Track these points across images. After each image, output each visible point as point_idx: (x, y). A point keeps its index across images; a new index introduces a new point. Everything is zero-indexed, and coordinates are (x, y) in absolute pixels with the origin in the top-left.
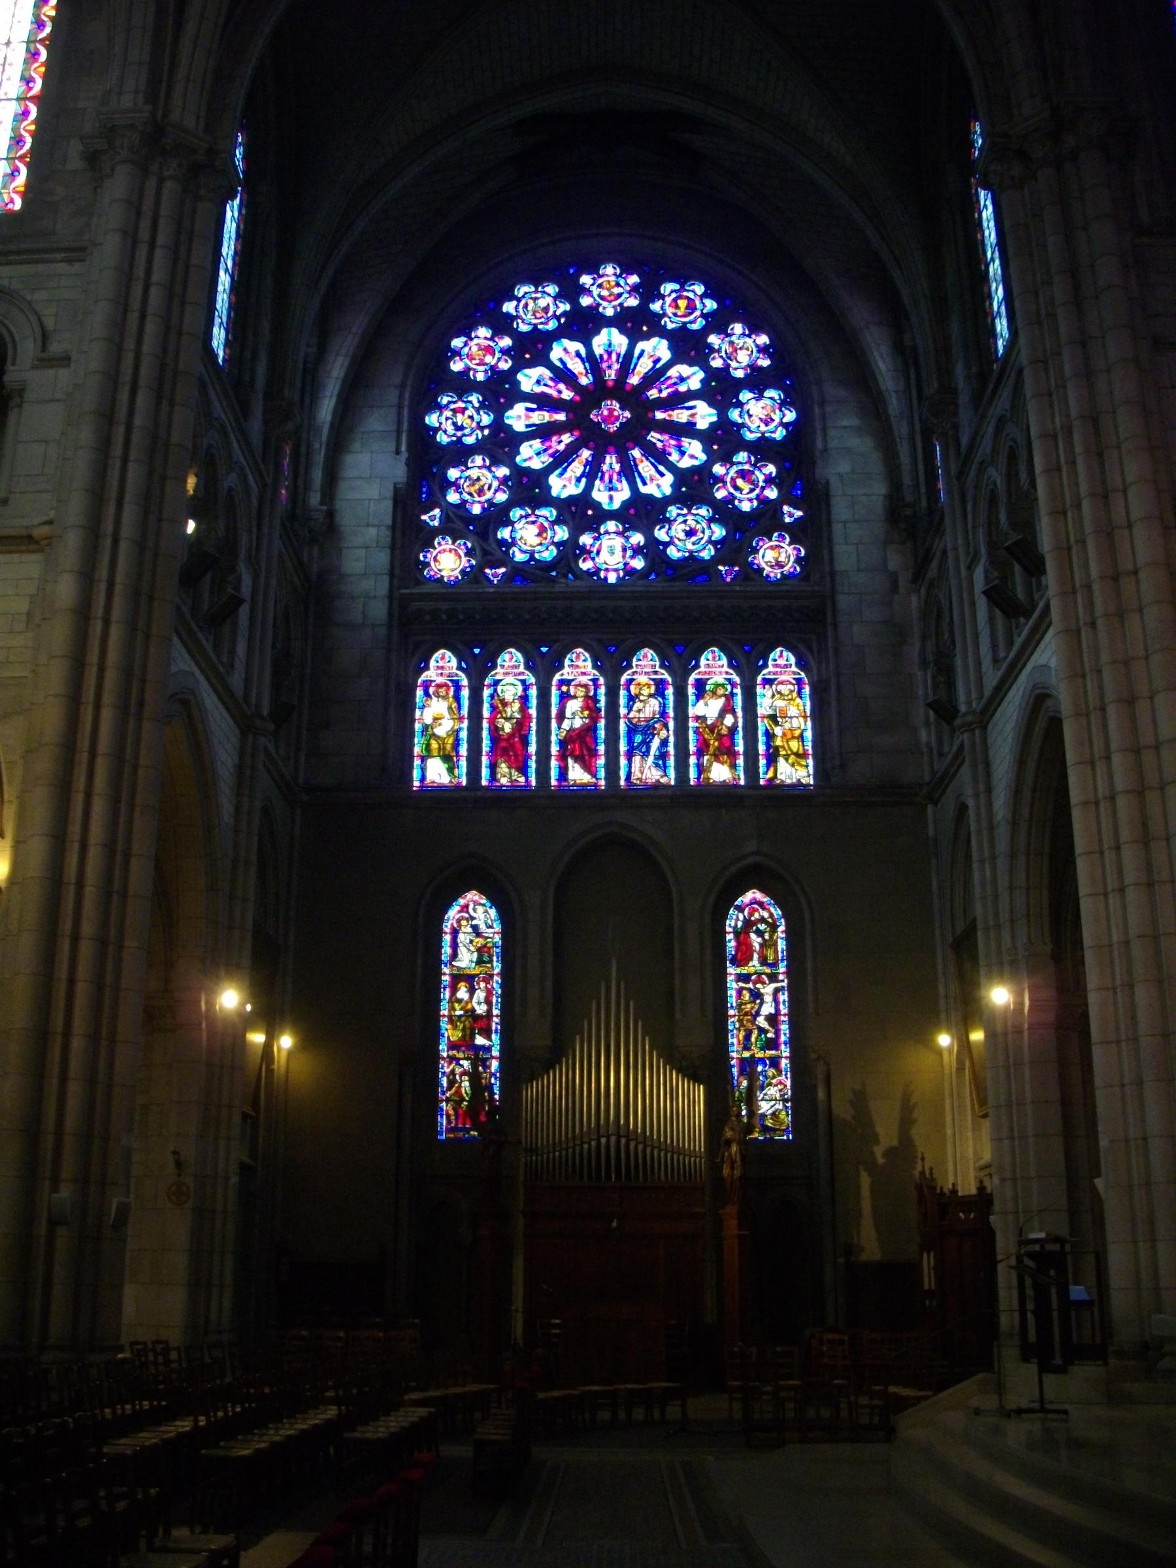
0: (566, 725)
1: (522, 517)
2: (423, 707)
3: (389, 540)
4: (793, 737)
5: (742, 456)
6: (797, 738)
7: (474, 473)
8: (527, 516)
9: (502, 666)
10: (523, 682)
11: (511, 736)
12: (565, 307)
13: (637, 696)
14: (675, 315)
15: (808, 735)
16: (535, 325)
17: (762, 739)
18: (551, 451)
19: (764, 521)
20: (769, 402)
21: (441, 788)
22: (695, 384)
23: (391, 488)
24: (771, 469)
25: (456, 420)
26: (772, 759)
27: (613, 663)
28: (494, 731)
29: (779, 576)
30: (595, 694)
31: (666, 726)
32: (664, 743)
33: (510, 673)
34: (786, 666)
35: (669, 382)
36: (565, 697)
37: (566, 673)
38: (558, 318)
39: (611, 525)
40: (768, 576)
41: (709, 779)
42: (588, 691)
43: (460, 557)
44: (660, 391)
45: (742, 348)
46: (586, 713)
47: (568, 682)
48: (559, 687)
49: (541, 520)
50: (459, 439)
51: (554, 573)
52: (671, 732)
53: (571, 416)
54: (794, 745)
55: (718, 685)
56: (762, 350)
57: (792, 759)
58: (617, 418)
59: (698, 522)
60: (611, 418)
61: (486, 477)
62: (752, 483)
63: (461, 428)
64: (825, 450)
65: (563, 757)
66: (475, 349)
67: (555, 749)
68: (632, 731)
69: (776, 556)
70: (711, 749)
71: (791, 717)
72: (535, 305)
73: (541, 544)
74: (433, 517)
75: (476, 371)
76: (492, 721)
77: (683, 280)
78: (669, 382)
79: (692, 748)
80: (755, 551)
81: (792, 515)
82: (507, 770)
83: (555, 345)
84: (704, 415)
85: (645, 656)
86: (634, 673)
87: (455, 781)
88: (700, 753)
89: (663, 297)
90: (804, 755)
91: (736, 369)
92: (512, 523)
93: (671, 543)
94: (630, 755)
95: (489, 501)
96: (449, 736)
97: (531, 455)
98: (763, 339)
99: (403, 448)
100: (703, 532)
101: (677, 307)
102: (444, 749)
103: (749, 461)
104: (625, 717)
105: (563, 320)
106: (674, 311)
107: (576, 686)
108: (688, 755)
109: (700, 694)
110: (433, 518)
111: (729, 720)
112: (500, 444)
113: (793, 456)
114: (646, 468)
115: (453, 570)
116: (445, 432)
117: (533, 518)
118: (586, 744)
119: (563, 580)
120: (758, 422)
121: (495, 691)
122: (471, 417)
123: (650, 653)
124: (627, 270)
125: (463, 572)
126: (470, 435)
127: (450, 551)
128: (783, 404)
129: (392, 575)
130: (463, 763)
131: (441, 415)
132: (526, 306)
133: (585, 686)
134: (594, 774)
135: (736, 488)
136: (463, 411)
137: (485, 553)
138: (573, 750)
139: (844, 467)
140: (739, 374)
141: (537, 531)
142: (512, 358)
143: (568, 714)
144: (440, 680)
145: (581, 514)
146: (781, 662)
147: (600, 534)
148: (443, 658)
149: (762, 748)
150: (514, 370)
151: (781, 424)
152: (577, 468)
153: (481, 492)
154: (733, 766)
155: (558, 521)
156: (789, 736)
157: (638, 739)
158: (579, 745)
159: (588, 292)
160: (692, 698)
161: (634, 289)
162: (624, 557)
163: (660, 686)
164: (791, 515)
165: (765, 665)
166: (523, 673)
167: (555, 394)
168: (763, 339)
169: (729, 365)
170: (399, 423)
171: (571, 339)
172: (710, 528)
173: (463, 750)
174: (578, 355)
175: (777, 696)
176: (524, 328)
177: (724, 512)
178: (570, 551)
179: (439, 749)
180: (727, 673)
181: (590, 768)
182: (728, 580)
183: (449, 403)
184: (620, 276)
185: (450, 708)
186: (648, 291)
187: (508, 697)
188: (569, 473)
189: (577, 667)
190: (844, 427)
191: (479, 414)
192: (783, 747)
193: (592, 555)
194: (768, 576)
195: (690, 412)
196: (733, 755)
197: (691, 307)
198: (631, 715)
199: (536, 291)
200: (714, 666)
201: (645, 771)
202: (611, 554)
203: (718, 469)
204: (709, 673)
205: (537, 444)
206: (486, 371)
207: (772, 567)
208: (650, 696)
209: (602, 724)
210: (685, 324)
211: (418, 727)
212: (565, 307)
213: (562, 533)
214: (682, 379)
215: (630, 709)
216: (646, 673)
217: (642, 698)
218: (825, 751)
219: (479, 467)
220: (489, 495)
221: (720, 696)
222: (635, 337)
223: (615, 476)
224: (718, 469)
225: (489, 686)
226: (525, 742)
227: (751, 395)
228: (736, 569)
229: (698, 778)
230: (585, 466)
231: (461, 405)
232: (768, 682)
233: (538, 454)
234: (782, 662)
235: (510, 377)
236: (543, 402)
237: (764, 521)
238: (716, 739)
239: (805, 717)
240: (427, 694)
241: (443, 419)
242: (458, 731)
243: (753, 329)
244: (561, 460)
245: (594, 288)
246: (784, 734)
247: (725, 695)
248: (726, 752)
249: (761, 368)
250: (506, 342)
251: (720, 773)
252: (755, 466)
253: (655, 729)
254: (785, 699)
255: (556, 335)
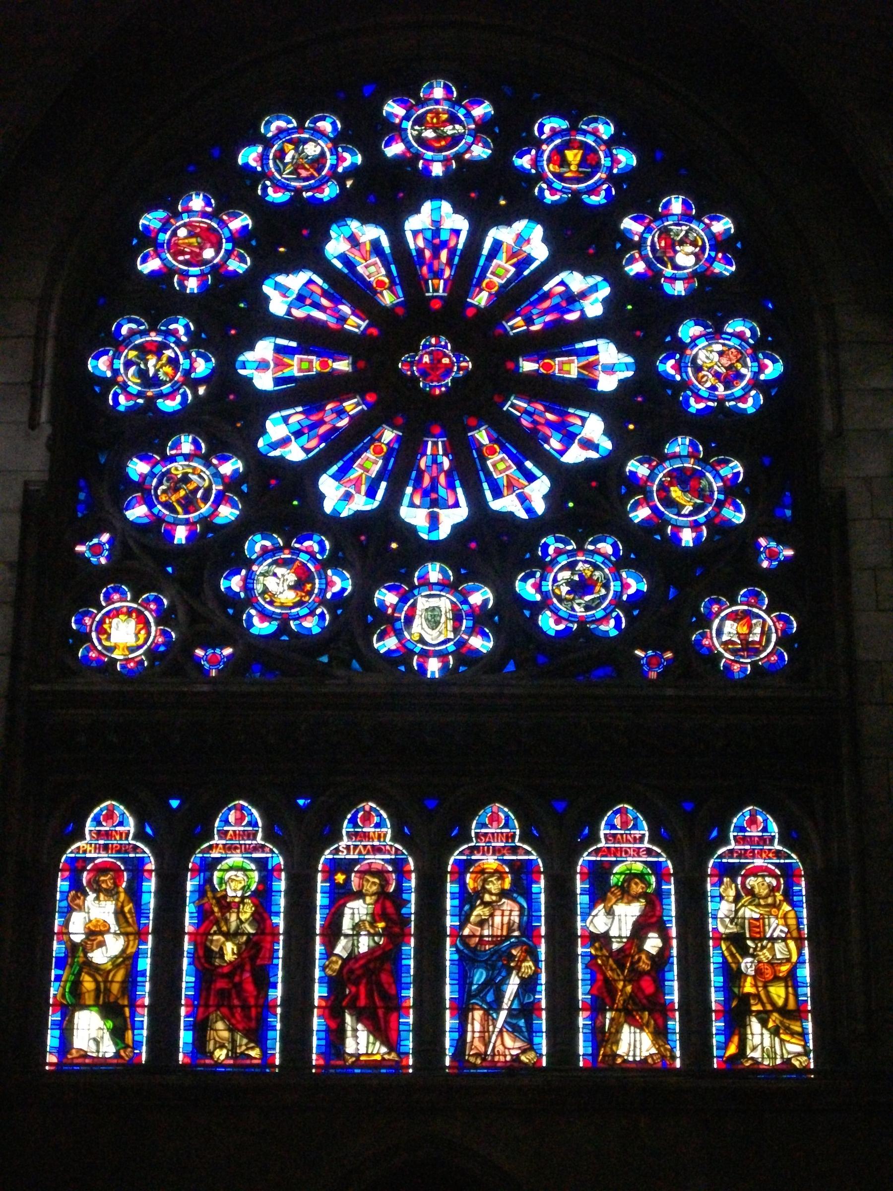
0: (341, 948)
1: (265, 552)
2: (70, 910)
3: (12, 589)
4: (776, 979)
5: (680, 445)
6: (784, 979)
7: (178, 468)
8: (277, 550)
9: (223, 834)
10: (262, 864)
11: (237, 966)
12: (352, 159)
13: (479, 894)
14: (560, 177)
15: (805, 973)
16: (298, 191)
17: (716, 980)
18: (322, 430)
19: (723, 565)
20: (734, 342)
21: (95, 1068)
22: (593, 308)
23: (18, 490)
24: (736, 467)
25: (144, 367)
26: (736, 1023)
27: (433, 833)
28: (205, 957)
29: (404, 962)
30: (399, 889)
31: (532, 954)
32: (528, 985)
33: (238, 859)
34: (762, 840)
35: (546, 304)
36: (341, 895)
37: (344, 846)
38: (341, 179)
39: (434, 572)
40: (727, 668)
41: (615, 1056)
42: (385, 883)
43: (147, 624)
44: (529, 321)
45: (687, 244)
46: (381, 925)
47: (347, 866)
48: (329, 877)
49: (304, 558)
50: (151, 402)
51: (325, 659)
52: (543, 965)
53: (362, 364)
54: (778, 992)
55: (631, 876)
56: (719, 243)
57: (775, 1019)
58: (448, 370)
59: (596, 567)
60: (435, 370)
61: (201, 476)
62: (699, 493)
63: (155, 382)
64: (839, 432)
65: (334, 1010)
66: (182, 233)
67: (319, 991)
68: (469, 958)
69: (740, 631)
70: (620, 1000)
71: (772, 940)
72: (294, 153)
73: (300, 604)
74: (96, 549)
75: (185, 275)
76: (201, 938)
77: (575, 115)
78: (546, 304)
79: (582, 993)
80: (705, 621)
81: (771, 552)
82: (226, 1034)
83: (334, 231)
84: (612, 365)
85: (494, 818)
86: (473, 850)
87: (126, 1054)
88: (596, 1008)
89: (538, 144)
90: (798, 1014)
91: (673, 279)
92: (248, 563)
93: (545, 603)
94: (462, 1010)
95: (203, 520)
96: (116, 966)
97: (283, 436)
98: (723, 225)
99: (44, 415)
100: (606, 586)
101: (564, 163)
102: (108, 991)
103: (694, 455)
104: (457, 932)
105: (349, 184)
106: (557, 169)
107: (362, 873)
108: (573, 1011)
109: (600, 891)
110: (97, 550)
111: (653, 944)
112: (228, 414)
113: (778, 447)
114: (500, 465)
115: (132, 650)
116: (124, 387)
117: (286, 555)
118: (379, 984)
119: (341, 672)
120: (711, 381)
121: (209, 881)
122: (173, 362)
123: (504, 811)
124: (471, 93)
125: (152, 653)
126: (170, 396)
127: (129, 612)
128: (759, 347)
129: (15, 657)
130: (143, 1018)
131: (117, 356)
132: (281, 154)
133: (380, 874)
134: (393, 1045)
135: (670, 503)
136: (159, 349)
137: (194, 617)
138: (355, 997)
139: (874, 464)
140: (679, 289)
141: (292, 578)
142: (251, 251)
143: (347, 925)
144: (103, 857)
145: (379, 549)
146: (754, 833)
147: (413, 587)
148: (110, 816)
149: (715, 997)
150: (257, 276)
151: (755, 383)
152: (371, 463)
153: (189, 504)
154: (660, 1034)
155: (335, 561)
156: (769, 975)
157: (479, 976)
158: (366, 988)
159: (397, 132)
160: (582, 900)
161: (483, 128)
162: (456, 630)
163: (522, 875)
164: (772, 556)
165: (723, 840)
166: (262, 848)
167: (331, 321)
168: (723, 225)
169: (660, 274)
170: (38, 367)
171: (364, 221)
172: (618, 578)
173: (145, 990)
174: (376, 245)
175: (746, 899)
176: (276, 197)
177: (647, 548)
178: (355, 619)
179: (97, 990)
180: (649, 852)
181: (382, 1031)
182: (653, 675)
183: (132, 333)
184: (457, 103)
185: (119, 913)
186: (509, 132)
187: (233, 892)
188: (356, 472)
189: (366, 836)
190: (876, 391)
191: (188, 356)
192: (757, 996)
193: (398, 625)
194: (727, 668)
195: (584, 361)
196: (662, 1011)
197: (590, 163)
198: (466, 932)
199: (301, 128)
200: (627, 840)
201: (495, 1038)
202: (432, 623)
203: (637, 468)
204: (616, 852)
205: (297, 416)
206: (202, 276)
207: (734, 652)
208: (503, 894)
209: (410, 948)
210: (577, 194)
211: (57, 948)
212: (352, 159)
213: (341, 582)
214: (571, 299)
215: (464, 920)
216: (496, 851)
217: (487, 898)
218: (834, 1008)
219: (187, 457)
220: (205, 509)
221: (636, 898)
222: (385, 520)
223: (442, 479)
224: (637, 468)
225: (196, 872)
226: (264, 983)
227: (698, 330)
228: (669, 655)
229: (595, 1054)
230: (386, 460)
231: (154, 337)
232: (727, 871)
233: (298, 434)
234: (755, 832)
235: (249, 288)
236: (309, 337)
237: (723, 565)
238: (627, 981)
239: (799, 941)
240: (76, 885)
241: (119, 364)
242: (136, 956)
243: (704, 206)
244: (340, 450)
245: (407, 125)
246: (759, 972)
247: (644, 895)
248: (647, 1008)
249: (719, 278)
250: (242, 221)
251: (635, 1044)
252: (704, 461)
253: (511, 957)
254: (760, 907)
255: (338, 211)
